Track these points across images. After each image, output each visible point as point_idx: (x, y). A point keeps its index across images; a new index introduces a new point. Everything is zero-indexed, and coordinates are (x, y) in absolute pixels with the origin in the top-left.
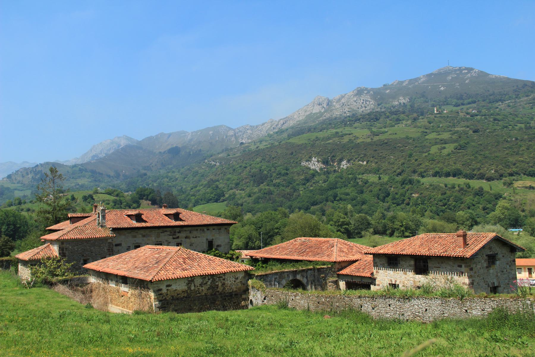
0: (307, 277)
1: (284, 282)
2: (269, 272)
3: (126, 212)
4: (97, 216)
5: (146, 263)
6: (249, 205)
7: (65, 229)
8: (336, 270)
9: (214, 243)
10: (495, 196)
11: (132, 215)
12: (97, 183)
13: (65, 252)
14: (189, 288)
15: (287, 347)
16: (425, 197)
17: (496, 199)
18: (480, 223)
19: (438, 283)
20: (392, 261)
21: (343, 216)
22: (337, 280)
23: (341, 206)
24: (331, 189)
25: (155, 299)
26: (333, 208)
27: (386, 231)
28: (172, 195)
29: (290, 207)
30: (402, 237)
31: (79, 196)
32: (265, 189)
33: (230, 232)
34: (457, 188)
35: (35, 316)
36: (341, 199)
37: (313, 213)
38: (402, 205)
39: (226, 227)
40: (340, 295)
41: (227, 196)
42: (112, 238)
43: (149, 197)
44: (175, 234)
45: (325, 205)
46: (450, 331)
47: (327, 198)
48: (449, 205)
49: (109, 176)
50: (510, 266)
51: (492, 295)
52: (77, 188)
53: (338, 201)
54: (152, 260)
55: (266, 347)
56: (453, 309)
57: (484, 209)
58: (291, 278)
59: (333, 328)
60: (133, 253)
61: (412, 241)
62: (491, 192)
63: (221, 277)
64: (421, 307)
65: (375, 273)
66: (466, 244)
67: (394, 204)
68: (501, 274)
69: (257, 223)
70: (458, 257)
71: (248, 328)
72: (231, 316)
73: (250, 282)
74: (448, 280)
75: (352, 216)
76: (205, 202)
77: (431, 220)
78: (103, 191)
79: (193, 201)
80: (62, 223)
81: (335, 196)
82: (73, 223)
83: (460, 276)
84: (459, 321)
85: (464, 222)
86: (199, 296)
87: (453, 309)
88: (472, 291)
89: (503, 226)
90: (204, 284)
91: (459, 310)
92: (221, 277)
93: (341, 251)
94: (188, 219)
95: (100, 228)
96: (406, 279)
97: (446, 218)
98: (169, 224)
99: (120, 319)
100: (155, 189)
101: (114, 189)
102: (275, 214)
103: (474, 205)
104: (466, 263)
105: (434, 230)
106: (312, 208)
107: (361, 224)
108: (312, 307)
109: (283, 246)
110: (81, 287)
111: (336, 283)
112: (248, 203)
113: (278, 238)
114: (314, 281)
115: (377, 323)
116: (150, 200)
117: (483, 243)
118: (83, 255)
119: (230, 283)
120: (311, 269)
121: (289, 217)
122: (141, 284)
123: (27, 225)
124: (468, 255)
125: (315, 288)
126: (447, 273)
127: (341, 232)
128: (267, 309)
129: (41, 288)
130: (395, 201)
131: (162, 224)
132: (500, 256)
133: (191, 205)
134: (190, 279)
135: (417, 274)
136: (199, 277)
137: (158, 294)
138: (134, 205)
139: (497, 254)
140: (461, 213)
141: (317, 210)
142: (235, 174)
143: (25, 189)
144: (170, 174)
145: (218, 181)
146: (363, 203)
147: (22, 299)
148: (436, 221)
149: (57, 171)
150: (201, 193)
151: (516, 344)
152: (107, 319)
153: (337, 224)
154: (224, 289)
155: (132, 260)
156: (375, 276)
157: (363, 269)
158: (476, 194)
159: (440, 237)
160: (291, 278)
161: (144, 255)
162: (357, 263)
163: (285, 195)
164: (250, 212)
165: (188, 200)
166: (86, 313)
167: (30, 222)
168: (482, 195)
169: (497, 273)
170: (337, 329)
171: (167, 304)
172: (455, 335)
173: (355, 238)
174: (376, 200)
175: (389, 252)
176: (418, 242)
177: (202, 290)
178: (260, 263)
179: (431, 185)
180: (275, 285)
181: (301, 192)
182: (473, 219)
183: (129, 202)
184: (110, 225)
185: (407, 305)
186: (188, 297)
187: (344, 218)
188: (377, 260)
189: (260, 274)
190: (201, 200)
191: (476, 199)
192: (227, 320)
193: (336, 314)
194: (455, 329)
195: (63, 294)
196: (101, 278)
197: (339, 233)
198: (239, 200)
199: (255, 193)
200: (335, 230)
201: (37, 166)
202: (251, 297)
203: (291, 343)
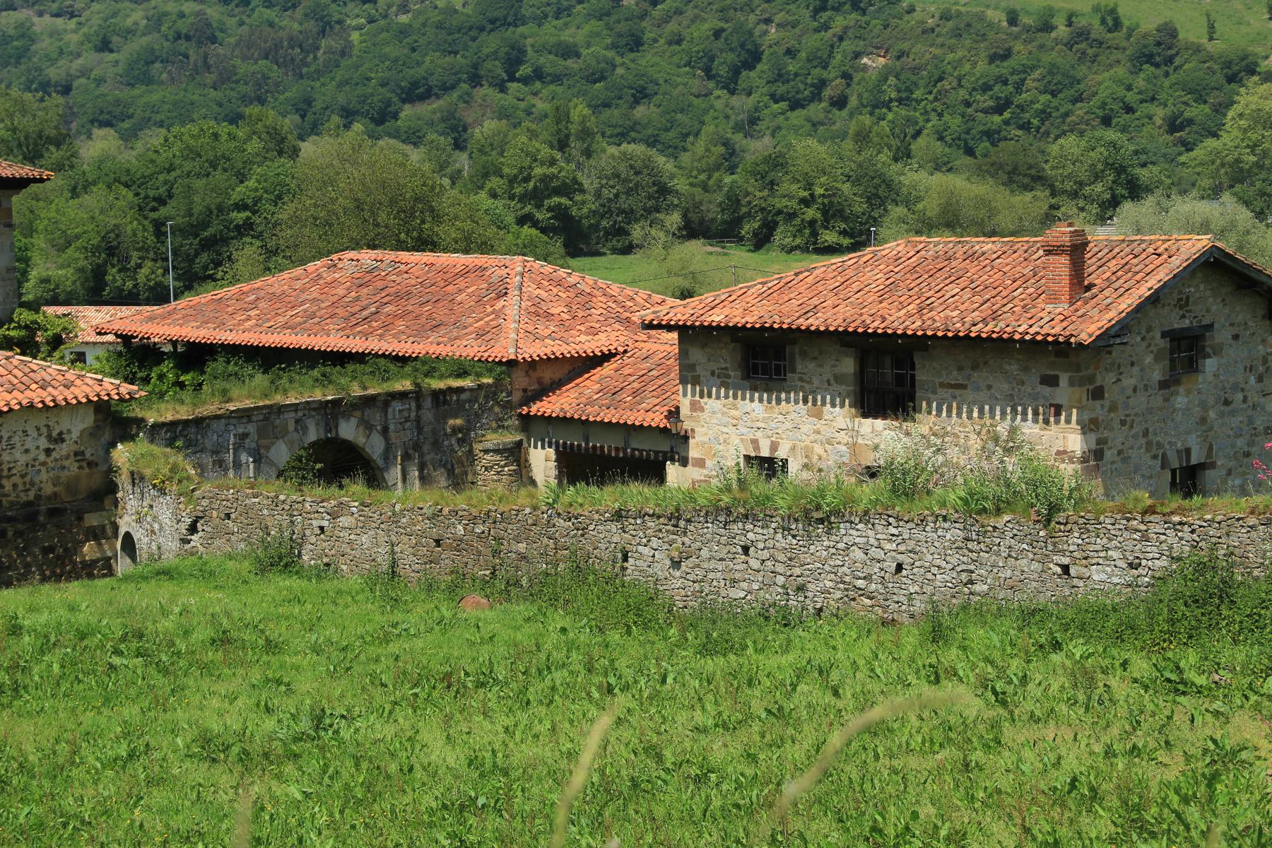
0: (385, 431)
1: (281, 453)
2: (210, 408)
6: (103, 89)
8: (517, 397)
10: (1228, 65)
15: (296, 739)
16: (915, 70)
17: (1232, 79)
18: (1149, 190)
19: (953, 453)
20: (764, 358)
21: (545, 152)
22: (519, 444)
23: (541, 106)
24: (495, 24)
26: (503, 114)
27: (737, 222)
29: (303, 107)
30: (805, 249)
32: (182, 15)
33: (16, 219)
34: (1062, 31)
36: (538, 75)
37: (414, 138)
38: (812, 107)
40: (535, 508)
45: (467, 100)
46: (996, 655)
47: (475, 66)
48: (1021, 108)
50: (1260, 379)
51: (1176, 501)
53: (525, 81)
55: (205, 740)
56: (1015, 565)
57: (1174, 125)
58: (313, 435)
59: (502, 650)
61: (850, 273)
62: (1210, 47)
64: (879, 554)
65: (685, 411)
66: (1080, 284)
67: (775, 99)
68: (1222, 415)
70: (1045, 342)
71: (116, 661)
72: (32, 609)
73: (122, 454)
74: (996, 439)
75: (588, 153)
77: (938, 178)
81: (514, 59)
83: (1046, 422)
84: (1033, 613)
85: (1081, 184)
87: (1015, 565)
88: (1096, 487)
89: (1247, 204)
91: (1036, 566)
93: (538, 312)
96: (819, 434)
97: (1001, 167)
102: (232, 137)
103: (1129, 109)
104: (1077, 368)
105: (950, 220)
106: (407, 111)
107: (628, 193)
108: (409, 563)
109: (277, 289)
111: (516, 454)
112: (100, 81)
113: (248, 251)
114: (417, 446)
115: (688, 625)
117: (1153, 282)
119: (23, 459)
120: (403, 395)
121: (295, 152)
124: (1087, 332)
125: (423, 479)
126: (992, 411)
127: (535, 224)
128: (206, 574)
130: (781, 89)
132: (1222, 335)
135: (865, 416)
139: (1210, 327)
140: (1070, 144)
141: (431, 124)
146: (641, 95)
148: (956, 182)
151: (1254, 698)
153: (518, 190)
156: (687, 425)
157: (635, 393)
158: (1145, 58)
159: (971, 256)
160: (313, 434)
162: (608, 369)
163: (277, 46)
164: (108, 124)
168: (1170, 60)
169: (1204, 406)
170: (518, 651)
172: (1015, 666)
173: (599, 254)
174: (697, 83)
175: (751, 320)
176: (876, 277)
178: (167, 366)
179: (945, 16)
180: (237, 465)
181: (355, 36)
182: (1121, 170)
185: (820, 548)
187: (553, 162)
188: (697, 355)
189: (169, 417)
191: (1140, 82)
192: (15, 630)
193: (513, 591)
194: (1013, 645)
197: (527, 231)
198: (53, 61)
199: (129, 31)
200: (510, 219)
202: (126, 524)
203: (318, 720)
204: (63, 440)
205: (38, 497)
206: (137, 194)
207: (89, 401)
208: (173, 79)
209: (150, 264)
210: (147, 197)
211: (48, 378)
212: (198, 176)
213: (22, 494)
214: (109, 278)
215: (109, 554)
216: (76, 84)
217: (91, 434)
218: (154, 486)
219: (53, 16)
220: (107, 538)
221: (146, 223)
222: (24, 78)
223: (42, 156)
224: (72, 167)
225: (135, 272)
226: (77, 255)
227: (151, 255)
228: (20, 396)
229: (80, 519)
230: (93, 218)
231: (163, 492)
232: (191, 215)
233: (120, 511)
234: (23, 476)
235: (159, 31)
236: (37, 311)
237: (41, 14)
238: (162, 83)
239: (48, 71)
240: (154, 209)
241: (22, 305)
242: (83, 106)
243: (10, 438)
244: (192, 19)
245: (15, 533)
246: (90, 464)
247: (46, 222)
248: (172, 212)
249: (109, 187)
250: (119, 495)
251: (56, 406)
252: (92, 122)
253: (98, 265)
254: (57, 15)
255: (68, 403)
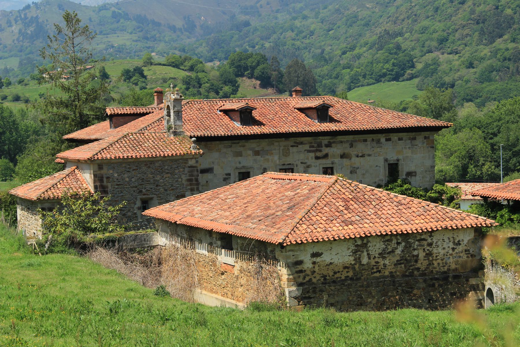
3: (220, 103)
4: (165, 112)
5: (269, 208)
6: (469, 85)
7: (104, 139)
9: (400, 168)
11: (233, 110)
12: (150, 44)
13: (105, 183)
14: (358, 260)
25: (289, 280)
28: (304, 67)
31: (115, 72)
32: (507, 49)
35: (62, 309)
39: (427, 134)
41: (419, 66)
42: (195, 157)
43: (257, 72)
44: (322, 148)
49: (173, 29)
52: (111, 54)
54: (280, 203)
60: (241, 188)
63: (424, 240)
69: (488, 125)
72: (451, 321)
76: (372, 81)
78: (163, 60)
79: (347, 78)
80: (93, 127)
82: (116, 127)
86: (377, 278)
90: (389, 253)
92: (424, 240)
94: (347, 118)
95: (172, 137)
98: (307, 129)
99: (227, 319)
100: (268, 55)
101: (184, 55)
110: (139, 253)
112: (467, 82)
116: (257, 79)
118: (141, 192)
119: (442, 252)
122: (260, 251)
123: (17, 129)
129: (65, 256)
131: (294, 129)
133: (341, 87)
134: (359, 243)
136: (378, 239)
137: (294, 270)
138: (227, 89)
142: (438, 18)
143: (6, 55)
144: (297, 23)
145: (401, 34)
147: (34, 275)
149: (78, 21)
150: (362, 60)
152: (200, 318)
154: (430, 264)
155: (240, 203)
161: (263, 191)
164: (471, 100)
165: (337, 78)
166: (158, 304)
167: (22, 125)
171: (314, 292)
177: (385, 265)
178: (504, 211)
183: (215, 83)
184: (190, 129)
186: (356, 279)
190: (364, 76)
192: (445, 330)
195: (108, 267)
196: (178, 236)
199: (482, 58)
201: (28, 7)
204: (460, 244)
205: (449, 270)
206: (484, 132)
207: (472, 227)
208: (501, 79)
209: (489, 164)
210: (488, 133)
211: (454, 216)
212: (513, 122)
213: (442, 268)
214: (469, 170)
215: (481, 298)
216: (456, 83)
217: (473, 242)
218: (503, 267)
219: (448, 54)
220: (480, 290)
221: (487, 144)
222: (434, 82)
223: (441, 116)
224: (454, 120)
225: (481, 167)
226: (455, 159)
227: (489, 159)
228: (441, 224)
229: (467, 281)
230: (463, 143)
231: (507, 270)
232: (508, 141)
233: (485, 278)
234: (442, 260)
235: (496, 57)
236: (444, 185)
237: (443, 54)
238: (496, 81)
239: (444, 78)
240: (491, 138)
241: (437, 182)
242: (459, 93)
243: (437, 242)
244: (512, 51)
245: (439, 285)
246: (472, 256)
247: (442, 145)
248: (500, 140)
249: (471, 129)
250: (485, 270)
251: (457, 228)
252: (463, 100)
253: (464, 164)
254: (450, 54)
255: (462, 227)
